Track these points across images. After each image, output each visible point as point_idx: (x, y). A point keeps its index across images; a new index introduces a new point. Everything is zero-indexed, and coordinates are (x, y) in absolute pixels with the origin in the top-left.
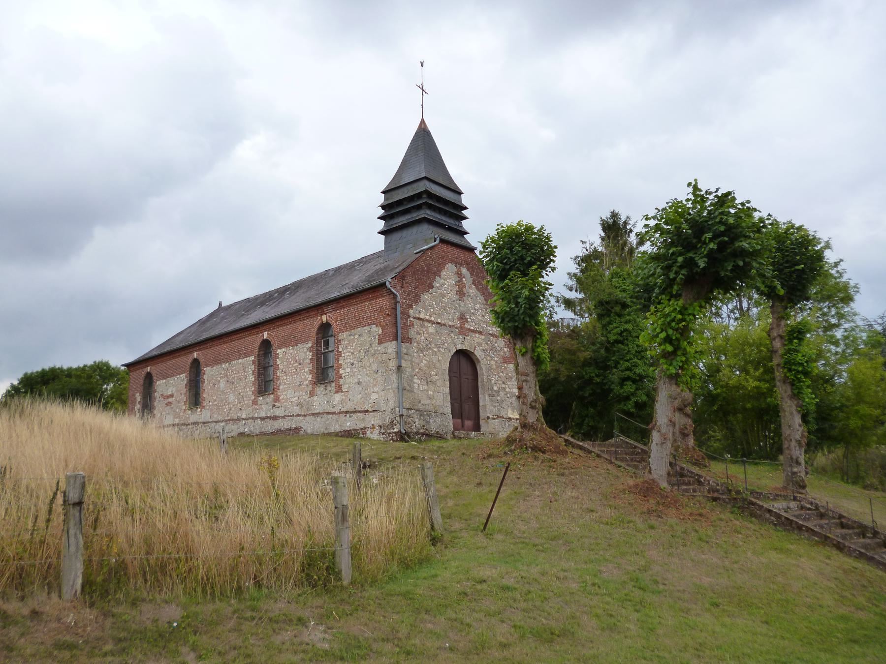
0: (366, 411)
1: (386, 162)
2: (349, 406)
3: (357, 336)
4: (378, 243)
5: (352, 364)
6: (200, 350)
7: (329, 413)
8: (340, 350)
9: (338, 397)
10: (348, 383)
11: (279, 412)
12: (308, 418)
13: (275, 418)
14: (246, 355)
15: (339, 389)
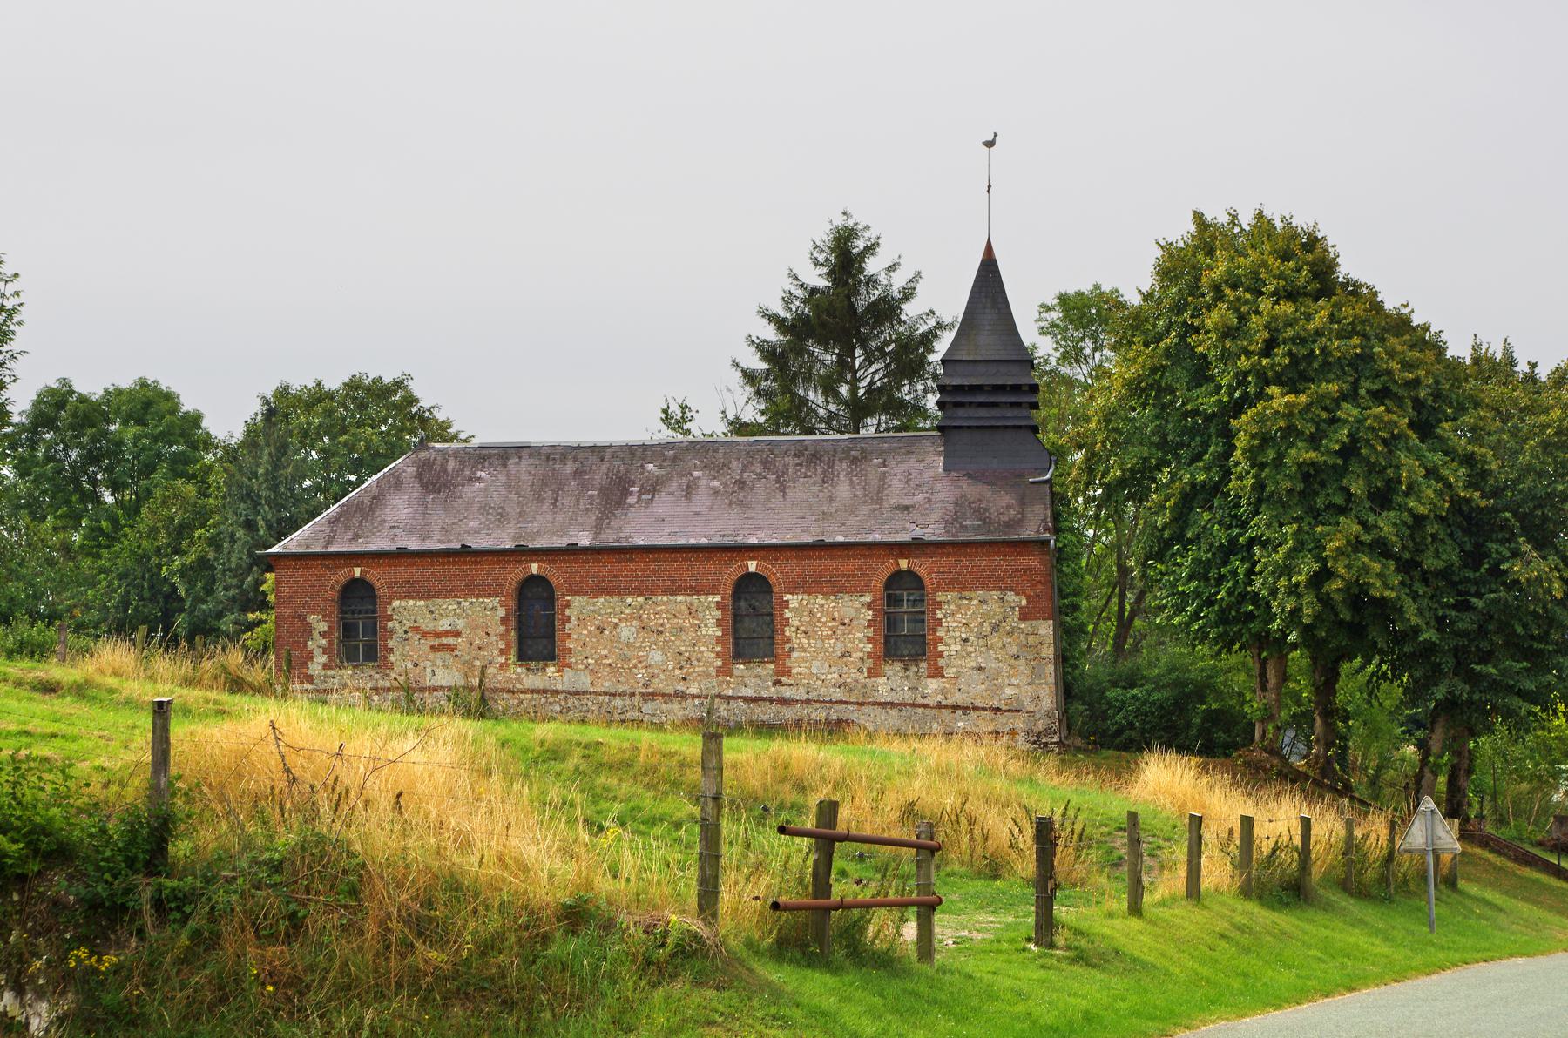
0: (998, 709)
1: (791, 267)
2: (958, 698)
3: (975, 602)
4: (721, 402)
5: (966, 640)
6: (543, 561)
7: (914, 705)
8: (939, 616)
9: (932, 685)
10: (798, 663)
11: (788, 693)
12: (865, 709)
13: (783, 701)
14: (713, 590)
15: (937, 673)
